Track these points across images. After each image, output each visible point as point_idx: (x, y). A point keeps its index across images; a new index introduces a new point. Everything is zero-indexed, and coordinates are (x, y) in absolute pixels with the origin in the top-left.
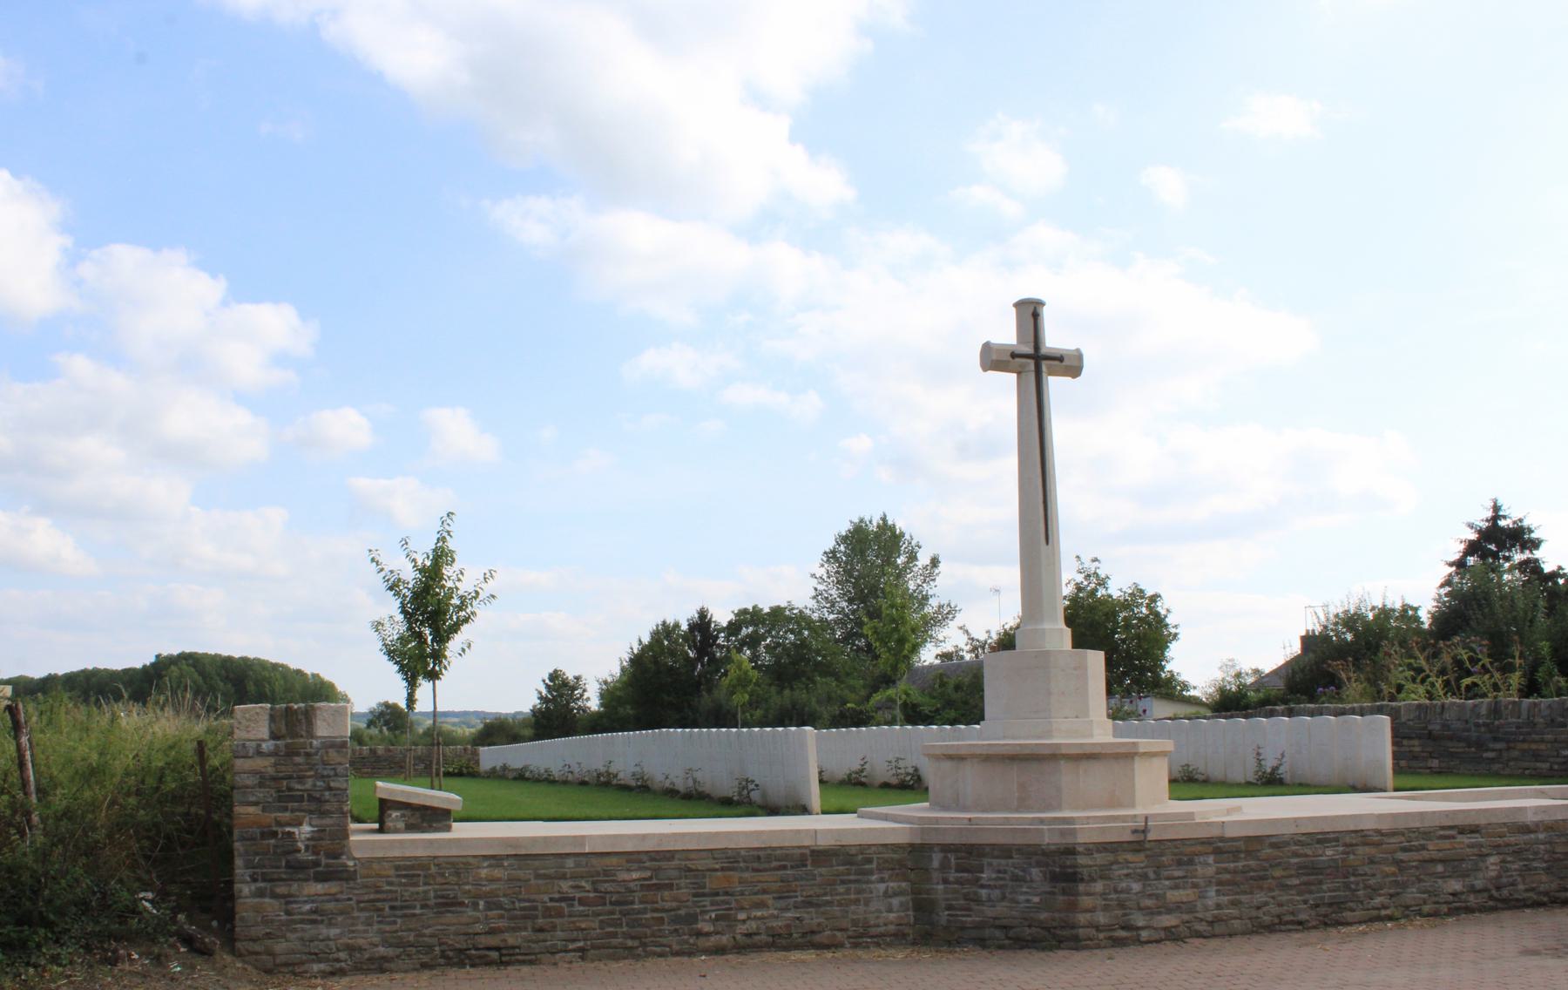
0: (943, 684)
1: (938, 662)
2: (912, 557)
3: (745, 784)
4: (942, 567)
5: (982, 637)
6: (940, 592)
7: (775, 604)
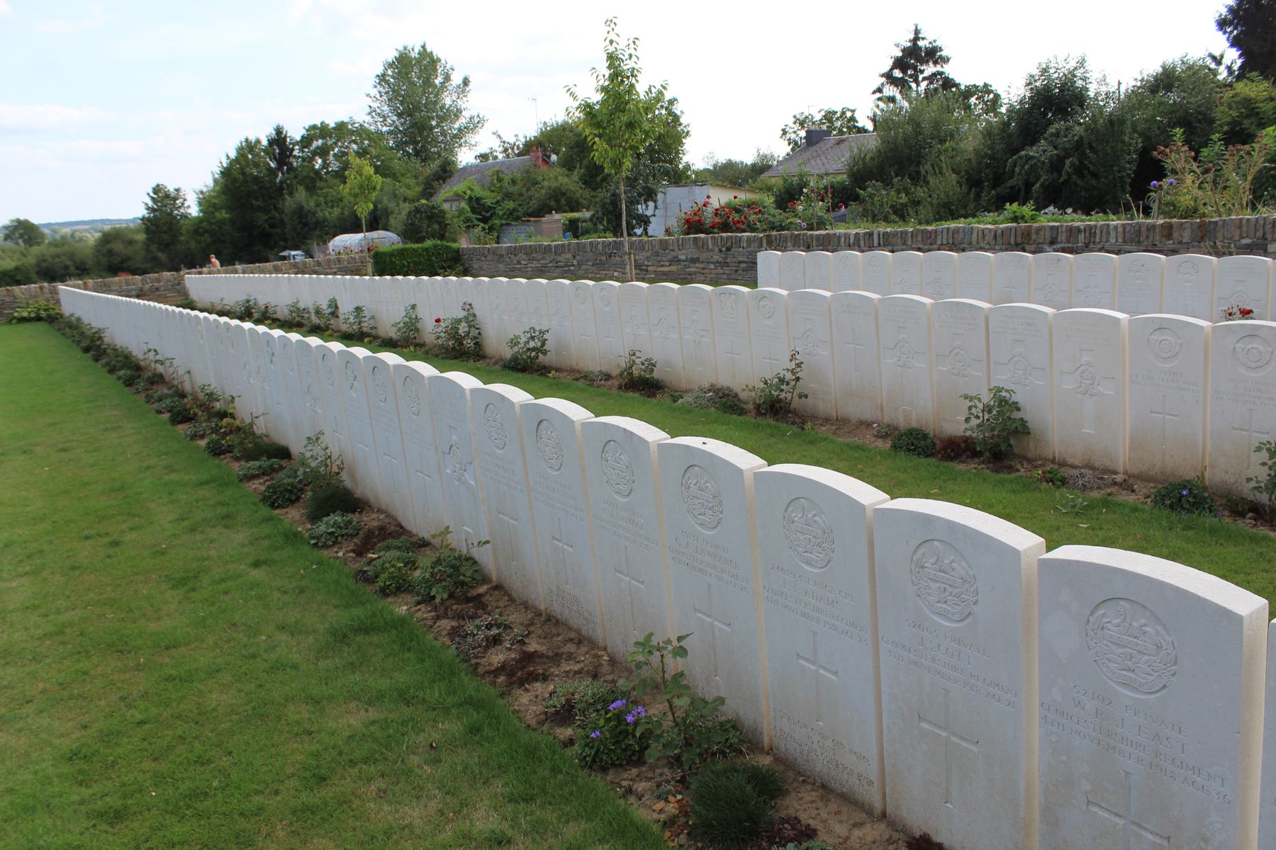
0: (500, 180)
2: (447, 78)
4: (471, 86)
5: (512, 140)
6: (471, 105)
7: (339, 119)
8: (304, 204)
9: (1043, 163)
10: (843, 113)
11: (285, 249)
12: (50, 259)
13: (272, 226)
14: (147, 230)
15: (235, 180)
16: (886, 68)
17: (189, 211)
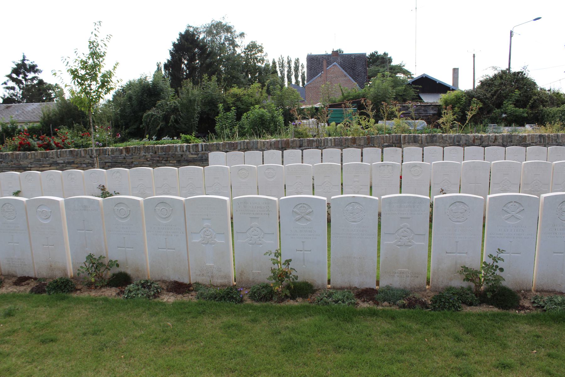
9: (159, 117)
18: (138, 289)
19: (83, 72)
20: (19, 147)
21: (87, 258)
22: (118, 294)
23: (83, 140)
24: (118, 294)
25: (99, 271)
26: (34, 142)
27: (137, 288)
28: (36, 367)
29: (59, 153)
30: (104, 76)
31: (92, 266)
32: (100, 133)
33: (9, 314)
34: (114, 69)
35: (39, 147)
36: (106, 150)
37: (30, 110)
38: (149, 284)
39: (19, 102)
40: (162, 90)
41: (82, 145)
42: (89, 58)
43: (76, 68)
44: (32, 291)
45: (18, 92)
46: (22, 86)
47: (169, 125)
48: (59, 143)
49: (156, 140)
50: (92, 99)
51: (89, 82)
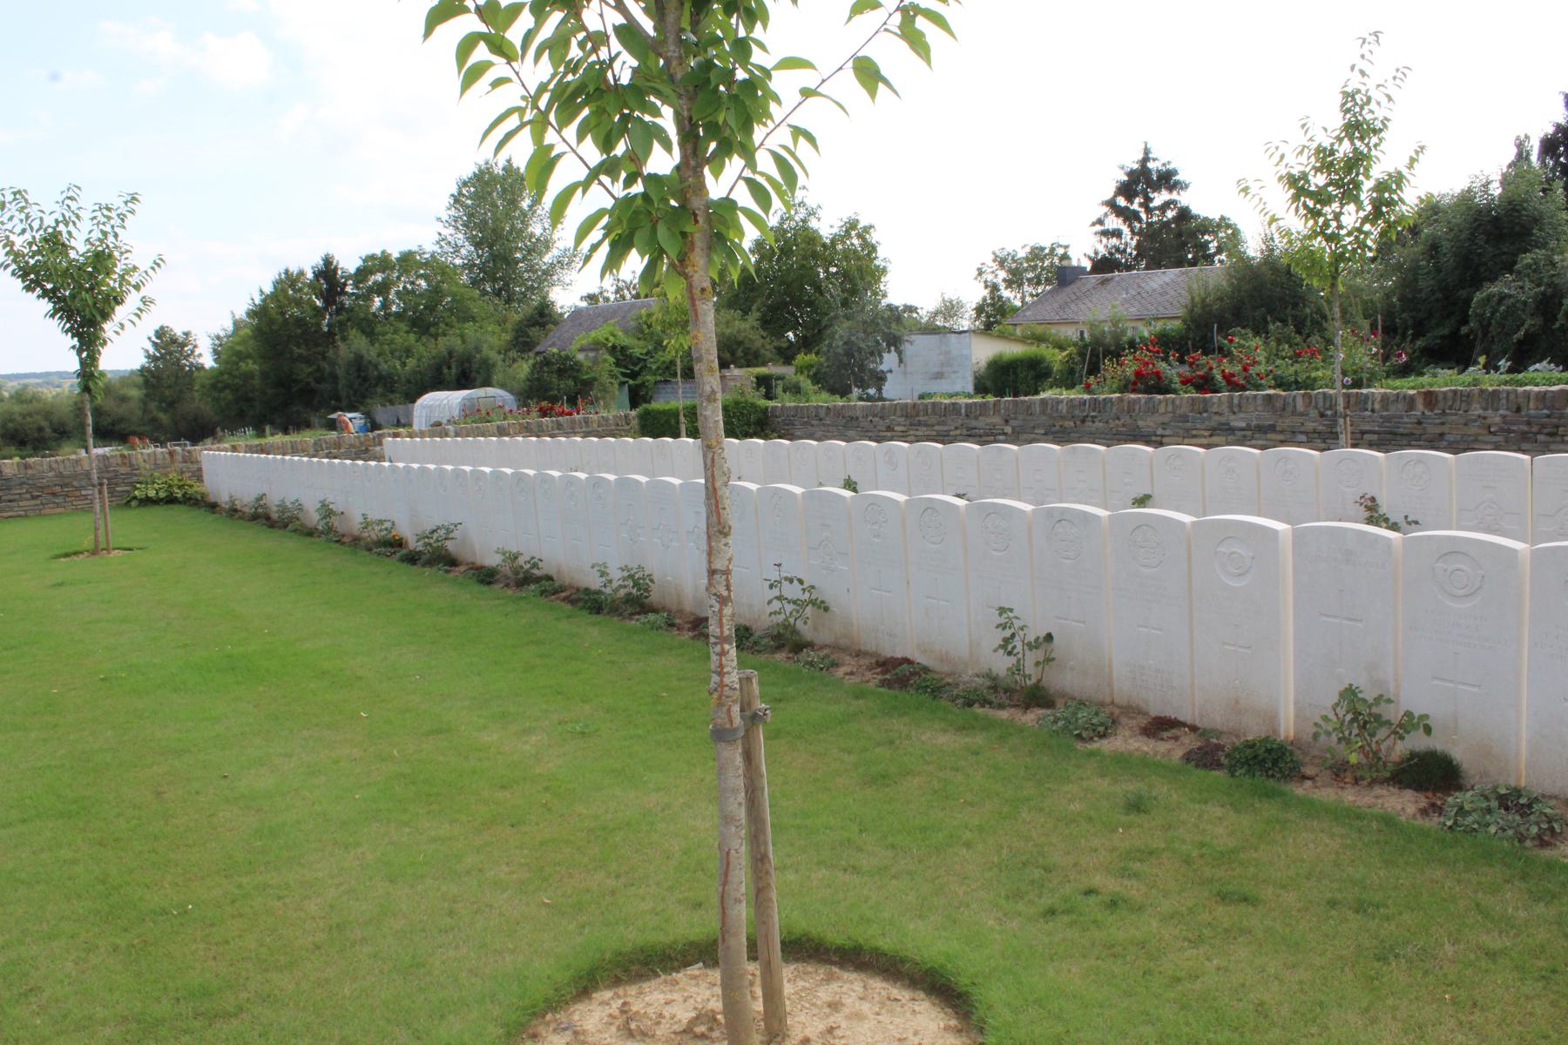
1: (584, 304)
3: (641, 582)
7: (405, 248)
8: (364, 352)
9: (1525, 303)
10: (1052, 250)
11: (335, 410)
12: (19, 419)
13: (318, 381)
14: (147, 383)
15: (272, 321)
16: (1109, 194)
17: (201, 360)
18: (1489, 811)
19: (1319, 180)
20: (1135, 383)
21: (1341, 695)
22: (1424, 812)
23: (1297, 366)
24: (1424, 812)
25: (1372, 735)
26: (1171, 370)
27: (1484, 805)
28: (1208, 959)
29: (1236, 401)
30: (1381, 187)
31: (1352, 721)
32: (1352, 349)
33: (1136, 806)
34: (1410, 167)
35: (1184, 383)
36: (1367, 396)
37: (1155, 286)
38: (1523, 801)
39: (1129, 268)
40: (1537, 220)
41: (1296, 382)
42: (1340, 140)
43: (1302, 168)
44: (1187, 757)
45: (1129, 240)
46: (1137, 225)
47: (1557, 325)
48: (1233, 375)
49: (1510, 371)
50: (1343, 254)
51: (1335, 206)
